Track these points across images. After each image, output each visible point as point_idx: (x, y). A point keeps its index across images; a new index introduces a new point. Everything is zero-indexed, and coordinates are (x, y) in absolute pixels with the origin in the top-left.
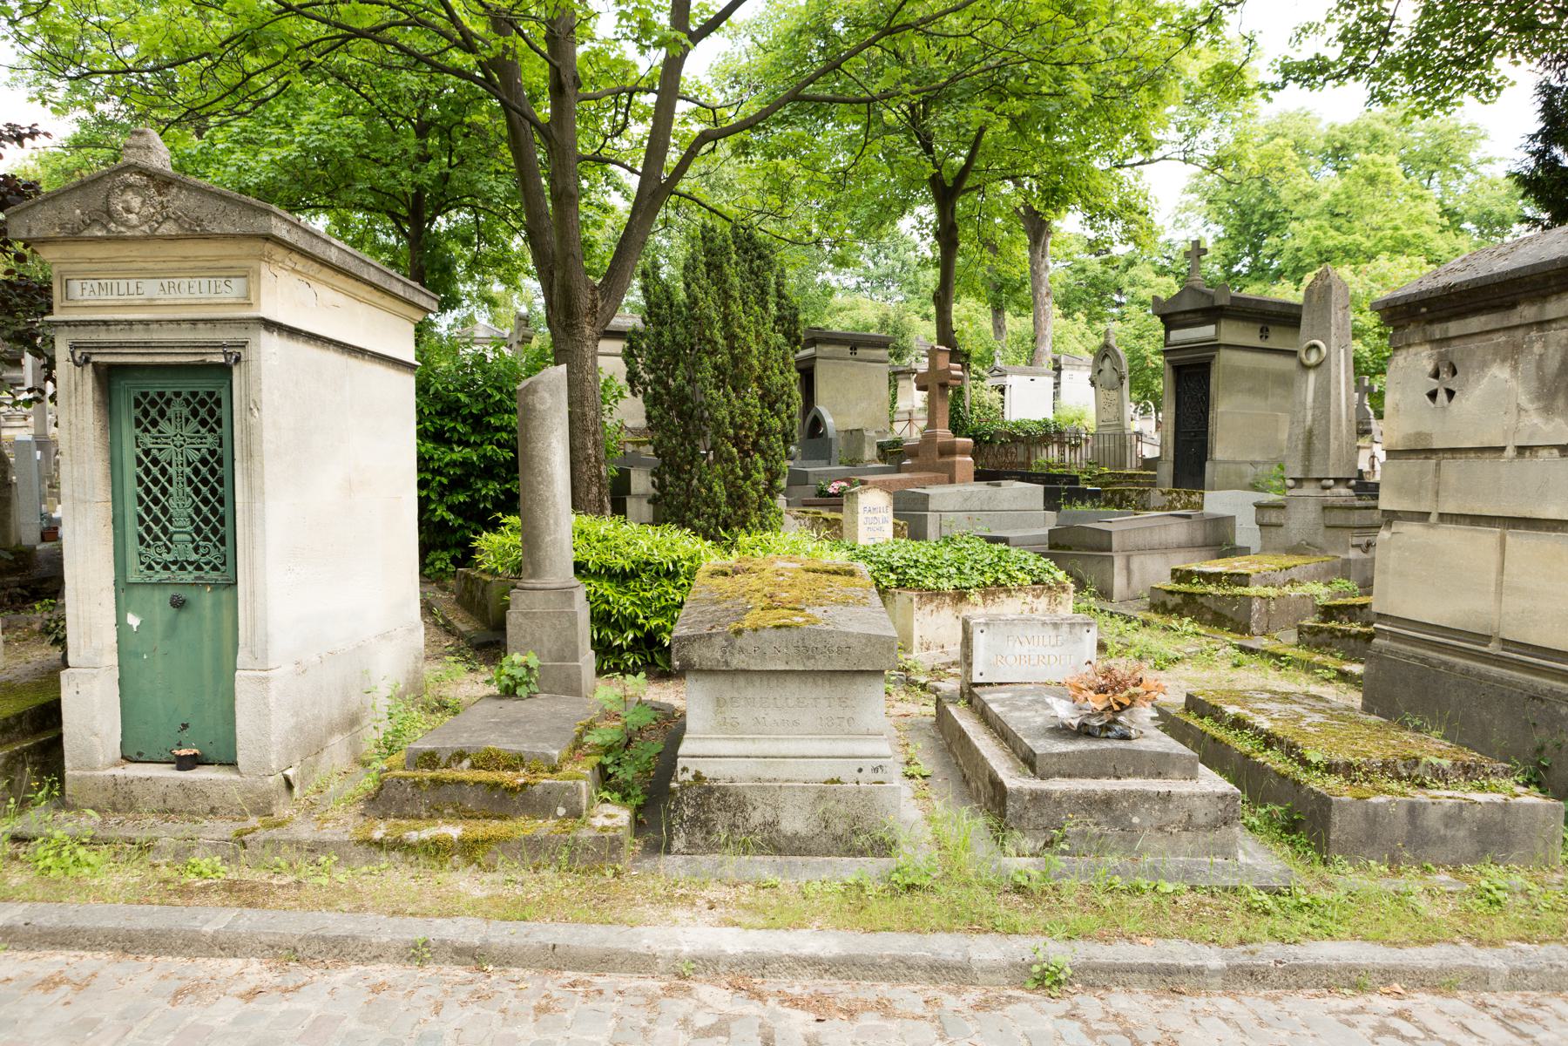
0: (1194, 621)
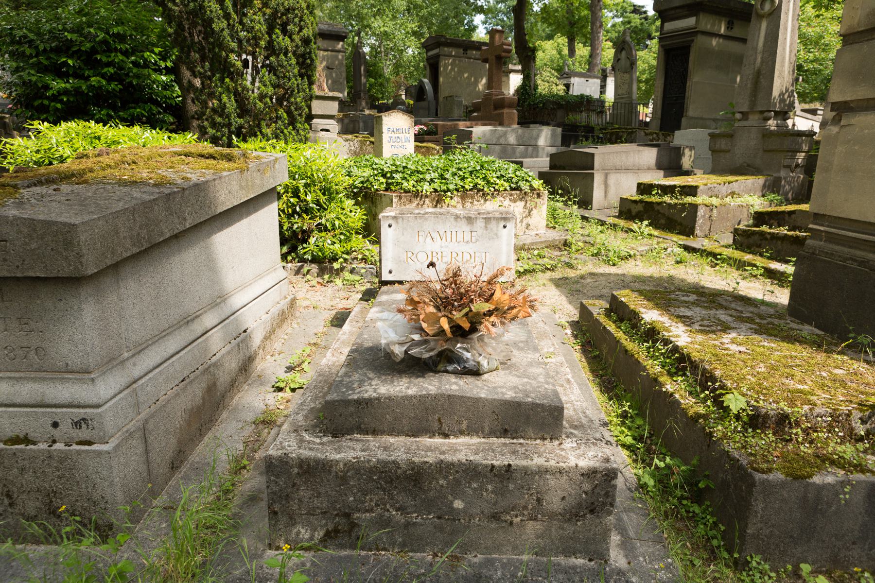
0: (650, 225)
